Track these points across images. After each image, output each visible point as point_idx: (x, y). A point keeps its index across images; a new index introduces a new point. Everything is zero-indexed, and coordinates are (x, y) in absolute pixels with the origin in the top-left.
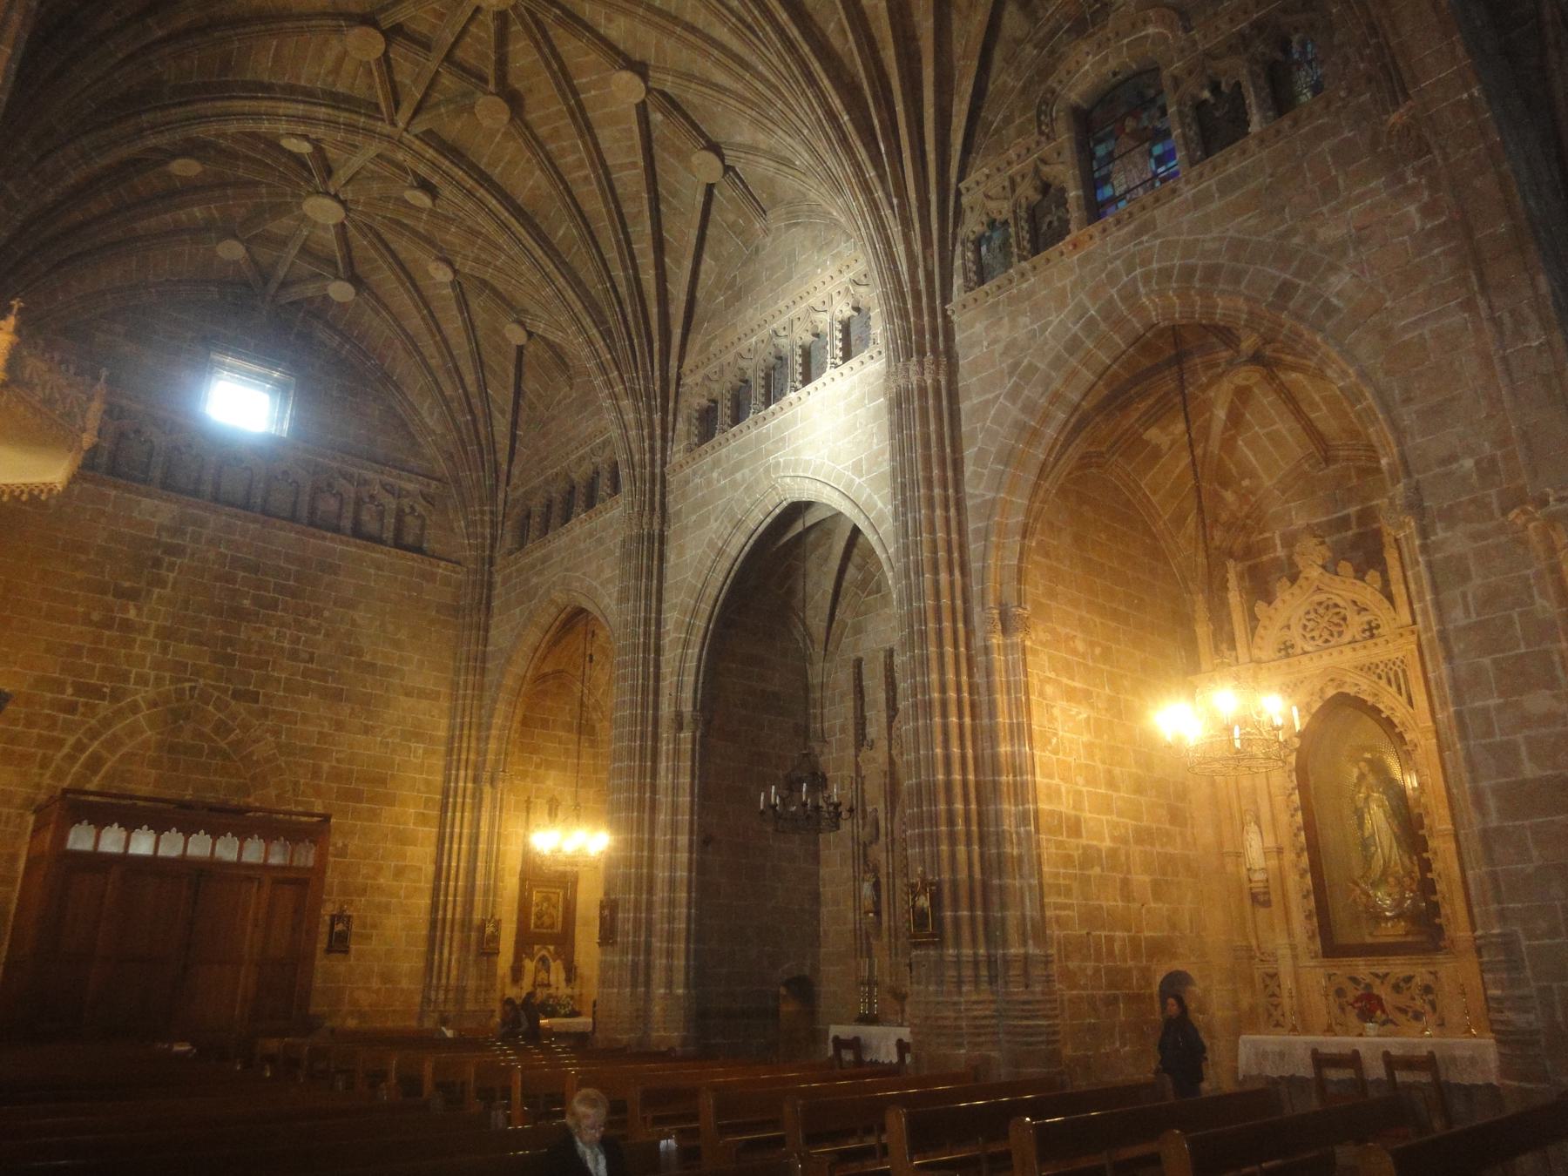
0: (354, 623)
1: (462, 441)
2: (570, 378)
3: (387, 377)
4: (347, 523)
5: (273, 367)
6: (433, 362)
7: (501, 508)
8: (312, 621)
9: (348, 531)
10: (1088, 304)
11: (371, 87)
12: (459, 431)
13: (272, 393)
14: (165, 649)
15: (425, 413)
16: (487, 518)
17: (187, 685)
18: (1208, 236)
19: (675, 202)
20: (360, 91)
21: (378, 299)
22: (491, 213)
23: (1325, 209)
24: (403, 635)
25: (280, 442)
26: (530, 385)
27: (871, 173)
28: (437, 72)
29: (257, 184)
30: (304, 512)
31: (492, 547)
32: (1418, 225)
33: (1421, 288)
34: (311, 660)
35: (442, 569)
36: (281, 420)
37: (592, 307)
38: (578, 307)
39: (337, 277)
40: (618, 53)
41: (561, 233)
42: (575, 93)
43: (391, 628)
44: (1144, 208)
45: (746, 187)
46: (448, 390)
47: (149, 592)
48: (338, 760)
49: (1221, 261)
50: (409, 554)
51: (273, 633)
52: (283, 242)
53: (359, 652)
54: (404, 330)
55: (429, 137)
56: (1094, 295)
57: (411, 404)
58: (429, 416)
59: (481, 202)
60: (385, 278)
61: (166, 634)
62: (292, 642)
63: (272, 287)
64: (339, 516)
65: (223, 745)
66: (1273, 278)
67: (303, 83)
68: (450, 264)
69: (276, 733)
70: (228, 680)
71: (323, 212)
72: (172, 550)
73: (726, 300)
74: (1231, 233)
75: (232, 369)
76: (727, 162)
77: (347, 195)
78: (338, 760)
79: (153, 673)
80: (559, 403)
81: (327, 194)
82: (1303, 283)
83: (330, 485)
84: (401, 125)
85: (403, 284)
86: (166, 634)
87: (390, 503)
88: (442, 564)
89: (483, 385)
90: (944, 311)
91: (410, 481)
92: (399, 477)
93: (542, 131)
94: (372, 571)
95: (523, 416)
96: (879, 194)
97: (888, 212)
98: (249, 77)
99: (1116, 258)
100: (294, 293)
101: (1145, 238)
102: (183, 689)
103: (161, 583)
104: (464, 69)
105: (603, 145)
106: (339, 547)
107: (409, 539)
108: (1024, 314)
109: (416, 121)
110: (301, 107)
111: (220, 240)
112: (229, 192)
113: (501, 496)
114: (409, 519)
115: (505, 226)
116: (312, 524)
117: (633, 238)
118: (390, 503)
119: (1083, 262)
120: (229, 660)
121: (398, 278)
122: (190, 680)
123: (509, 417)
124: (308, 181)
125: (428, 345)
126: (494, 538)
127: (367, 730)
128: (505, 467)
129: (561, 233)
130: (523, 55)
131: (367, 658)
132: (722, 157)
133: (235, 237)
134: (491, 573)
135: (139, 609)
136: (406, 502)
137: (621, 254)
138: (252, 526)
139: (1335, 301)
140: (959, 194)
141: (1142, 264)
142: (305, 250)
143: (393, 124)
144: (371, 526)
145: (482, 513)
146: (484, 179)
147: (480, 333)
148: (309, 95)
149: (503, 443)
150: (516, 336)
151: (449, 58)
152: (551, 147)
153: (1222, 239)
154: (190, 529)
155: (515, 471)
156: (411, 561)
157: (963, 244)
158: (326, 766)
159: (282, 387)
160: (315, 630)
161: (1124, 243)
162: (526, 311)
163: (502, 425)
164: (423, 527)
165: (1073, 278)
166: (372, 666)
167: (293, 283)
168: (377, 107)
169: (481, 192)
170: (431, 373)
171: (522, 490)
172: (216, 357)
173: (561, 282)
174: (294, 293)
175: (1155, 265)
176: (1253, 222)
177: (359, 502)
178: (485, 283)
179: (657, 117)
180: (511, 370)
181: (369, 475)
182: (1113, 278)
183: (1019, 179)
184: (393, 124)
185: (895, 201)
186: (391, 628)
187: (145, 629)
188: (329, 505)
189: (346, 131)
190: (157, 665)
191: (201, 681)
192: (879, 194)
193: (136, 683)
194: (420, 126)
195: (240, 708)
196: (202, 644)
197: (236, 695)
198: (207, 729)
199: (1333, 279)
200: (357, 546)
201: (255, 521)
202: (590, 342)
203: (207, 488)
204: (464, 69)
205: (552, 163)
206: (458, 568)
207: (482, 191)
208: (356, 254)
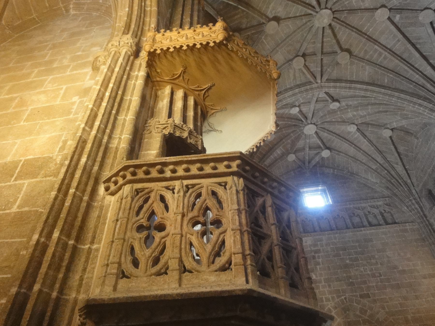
0: (388, 257)
1: (389, 181)
2: (415, 136)
3: (352, 174)
4: (366, 223)
5: (317, 186)
6: (364, 161)
7: (416, 196)
8: (373, 261)
9: (368, 225)
11: (306, 77)
12: (385, 178)
13: (321, 194)
14: (329, 286)
15: (370, 178)
16: (414, 201)
17: (343, 297)
19: (421, 41)
20: (304, 80)
21: (337, 151)
22: (360, 89)
24: (409, 256)
25: (330, 206)
26: (401, 149)
28: (322, 59)
29: (289, 134)
30: (350, 225)
31: (422, 211)
34: (381, 275)
35: (408, 226)
36: (328, 201)
37: (413, 95)
38: (408, 97)
39: (323, 150)
40: (372, 9)
41: (386, 81)
42: (366, 34)
43: (402, 254)
46: (374, 167)
47: (316, 268)
48: (412, 313)
50: (393, 225)
51: (362, 270)
52: (303, 149)
53: (395, 267)
54: (350, 156)
55: (328, 80)
57: (364, 178)
58: (373, 179)
59: (355, 88)
60: (337, 143)
61: (327, 281)
62: (370, 271)
63: (307, 164)
64: (362, 222)
65: (366, 318)
67: (288, 87)
68: (354, 124)
69: (383, 308)
70: (356, 292)
71: (310, 130)
72: (317, 252)
75: (307, 192)
77: (314, 120)
78: (412, 313)
79: (330, 296)
80: (416, 148)
81: (308, 124)
83: (354, 214)
84: (319, 81)
85: (342, 141)
86: (327, 281)
87: (376, 211)
88: (407, 224)
89: (385, 158)
91: (378, 201)
92: (374, 202)
93: (361, 55)
94: (383, 236)
95: (405, 161)
100: (313, 163)
102: (342, 299)
103: (318, 264)
104: (328, 53)
105: (384, 43)
106: (368, 232)
107: (390, 221)
109: (323, 78)
110: (291, 92)
111: (287, 156)
112: (284, 140)
113: (414, 191)
114: (385, 214)
115: (366, 90)
116: (354, 228)
117: (413, 64)
118: (376, 211)
120: (352, 284)
121: (340, 139)
122: (343, 296)
123: (400, 163)
124: (302, 124)
125: (360, 156)
126: (421, 208)
127: (417, 297)
128: (409, 181)
129: (386, 81)
130: (344, 35)
131: (401, 268)
132: (430, 9)
133: (291, 153)
134: (428, 221)
135: (316, 275)
136: (382, 209)
137: (413, 71)
138: (336, 235)
142: (310, 148)
143: (317, 83)
144: (374, 222)
145: (411, 200)
146: (352, 82)
147: (374, 142)
148: (291, 89)
149: (403, 173)
150: (387, 133)
151: (322, 53)
152: (367, 57)
154: (319, 243)
155: (414, 180)
156: (396, 228)
158: (409, 317)
159: (324, 191)
160: (377, 263)
162: (386, 124)
163: (400, 168)
164: (392, 215)
166: (404, 272)
167: (312, 160)
168: (310, 82)
169: (353, 85)
170: (366, 165)
171: (421, 185)
172: (302, 190)
173: (396, 94)
174: (313, 163)
177: (366, 215)
179: (397, 18)
180: (392, 147)
181: (363, 205)
184: (317, 83)
186: (402, 254)
187: (320, 282)
188: (356, 220)
189: (306, 92)
190: (330, 293)
191: (347, 295)
193: (326, 301)
194: (325, 77)
195: (365, 301)
196: (341, 281)
197: (361, 296)
198: (358, 313)
200: (374, 229)
201: (337, 233)
202: (420, 105)
203: (317, 228)
204: (328, 53)
205: (369, 61)
206: (414, 224)
207: (353, 85)
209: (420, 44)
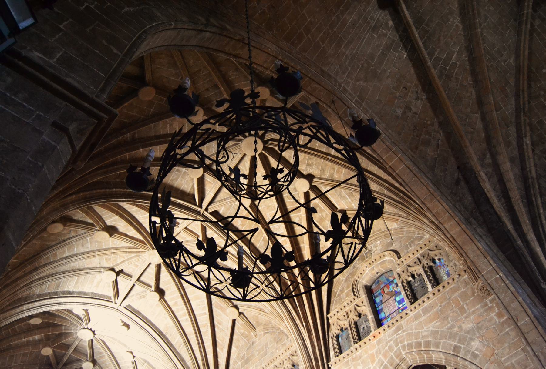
10: (384, 360)
18: (423, 330)
19: (220, 326)
23: (462, 317)
27: (294, 314)
32: (497, 320)
33: (506, 345)
44: (397, 321)
45: (248, 320)
49: (429, 339)
56: (385, 355)
66: (451, 345)
73: (242, 364)
74: (431, 328)
76: (240, 311)
82: (462, 346)
90: (328, 365)
96: (298, 321)
97: (302, 328)
98: (66, 289)
99: (391, 340)
101: (400, 332)
108: (359, 365)
119: (379, 342)
139: (476, 352)
140: (328, 319)
141: (401, 343)
153: (428, 331)
157: (332, 338)
161: (392, 335)
165: (376, 349)
175: (406, 343)
176: (438, 324)
178: (145, 361)
182: (391, 348)
183: (349, 312)
185: (304, 324)
192: (298, 321)
199: (473, 343)
208: (95, 351)
209: (218, 328)
